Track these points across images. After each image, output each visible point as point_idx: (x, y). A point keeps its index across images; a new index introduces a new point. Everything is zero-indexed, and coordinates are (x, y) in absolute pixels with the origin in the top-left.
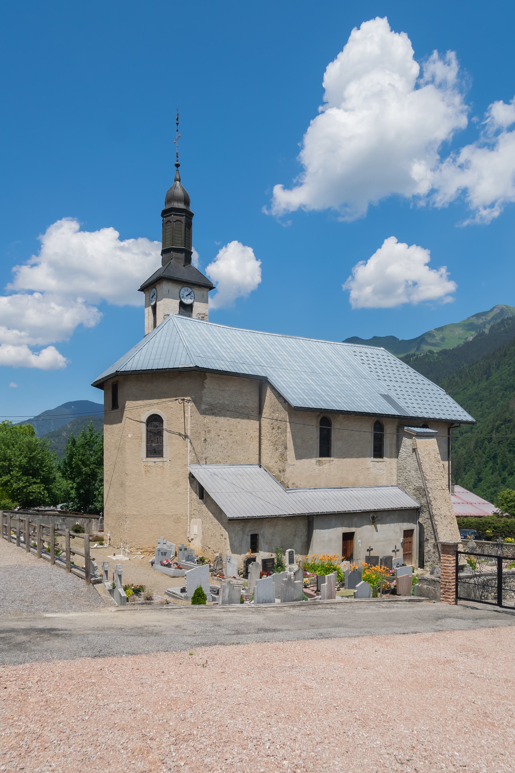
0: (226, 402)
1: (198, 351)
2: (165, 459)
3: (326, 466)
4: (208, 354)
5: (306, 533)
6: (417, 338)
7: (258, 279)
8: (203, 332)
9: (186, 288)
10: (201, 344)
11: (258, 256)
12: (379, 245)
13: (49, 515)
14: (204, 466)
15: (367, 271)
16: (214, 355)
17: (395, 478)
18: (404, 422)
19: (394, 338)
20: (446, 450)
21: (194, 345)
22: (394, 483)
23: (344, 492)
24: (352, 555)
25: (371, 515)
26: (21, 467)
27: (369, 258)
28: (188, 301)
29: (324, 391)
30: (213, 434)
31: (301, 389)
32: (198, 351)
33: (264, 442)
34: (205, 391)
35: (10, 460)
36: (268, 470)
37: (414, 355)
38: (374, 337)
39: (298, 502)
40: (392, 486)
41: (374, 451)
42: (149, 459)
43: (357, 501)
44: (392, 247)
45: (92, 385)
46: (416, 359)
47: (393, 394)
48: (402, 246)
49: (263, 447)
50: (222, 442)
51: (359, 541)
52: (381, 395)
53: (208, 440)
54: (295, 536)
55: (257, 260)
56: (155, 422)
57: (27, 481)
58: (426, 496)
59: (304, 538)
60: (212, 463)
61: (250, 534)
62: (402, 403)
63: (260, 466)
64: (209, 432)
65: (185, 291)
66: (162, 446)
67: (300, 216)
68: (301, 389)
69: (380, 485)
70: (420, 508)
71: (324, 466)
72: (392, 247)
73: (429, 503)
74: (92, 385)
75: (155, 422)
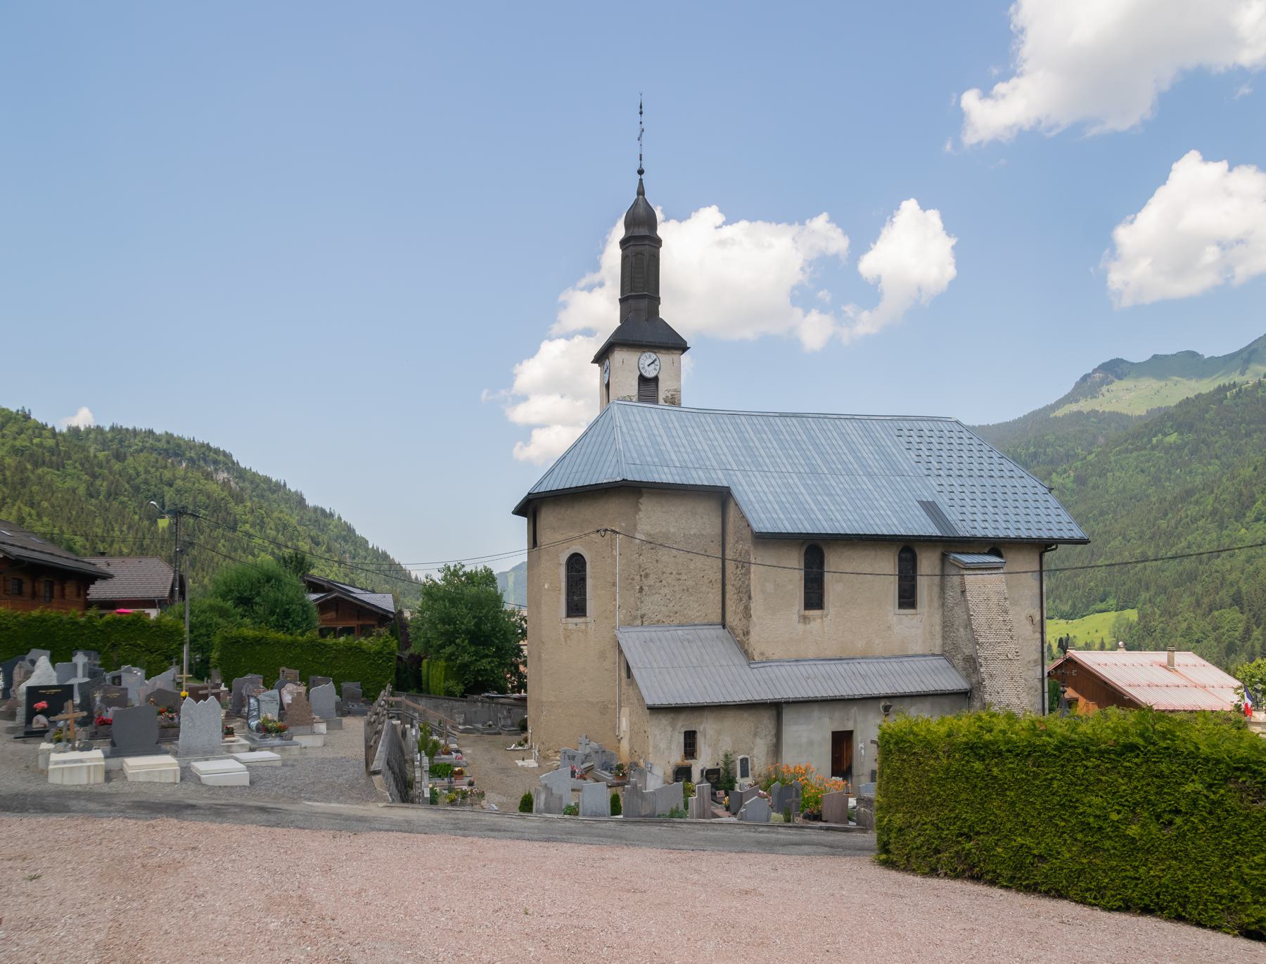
0: (672, 530)
1: (635, 455)
2: (588, 619)
3: (815, 626)
4: (649, 459)
5: (773, 732)
6: (1241, 351)
7: (951, 272)
8: (652, 424)
9: (647, 354)
10: (642, 443)
11: (949, 229)
12: (1162, 177)
13: (502, 704)
14: (639, 629)
15: (1142, 232)
16: (656, 460)
17: (939, 642)
18: (951, 546)
19: (1193, 354)
20: (1038, 591)
21: (631, 446)
22: (937, 651)
23: (846, 666)
24: (850, 768)
25: (882, 704)
26: (468, 632)
27: (1140, 210)
28: (650, 373)
29: (817, 502)
30: (651, 581)
31: (780, 503)
32: (635, 455)
33: (729, 588)
34: (641, 514)
35: (455, 624)
36: (732, 631)
37: (1234, 385)
38: (1155, 357)
39: (762, 683)
40: (933, 655)
41: (900, 597)
42: (570, 620)
43: (863, 682)
44: (1192, 174)
45: (514, 513)
46: (1237, 394)
47: (943, 502)
48: (1217, 169)
49: (728, 596)
50: (666, 591)
51: (861, 745)
52: (922, 503)
53: (646, 588)
54: (755, 735)
55: (948, 235)
56: (576, 565)
57: (476, 653)
58: (976, 670)
59: (770, 739)
60: (650, 625)
61: (683, 730)
62: (953, 516)
63: (724, 627)
64: (647, 576)
65: (647, 357)
66: (585, 600)
67: (1029, 142)
68: (780, 503)
69: (910, 653)
70: (971, 691)
71: (813, 624)
72: (1192, 174)
73: (980, 683)
74: (514, 513)
75: (576, 565)
